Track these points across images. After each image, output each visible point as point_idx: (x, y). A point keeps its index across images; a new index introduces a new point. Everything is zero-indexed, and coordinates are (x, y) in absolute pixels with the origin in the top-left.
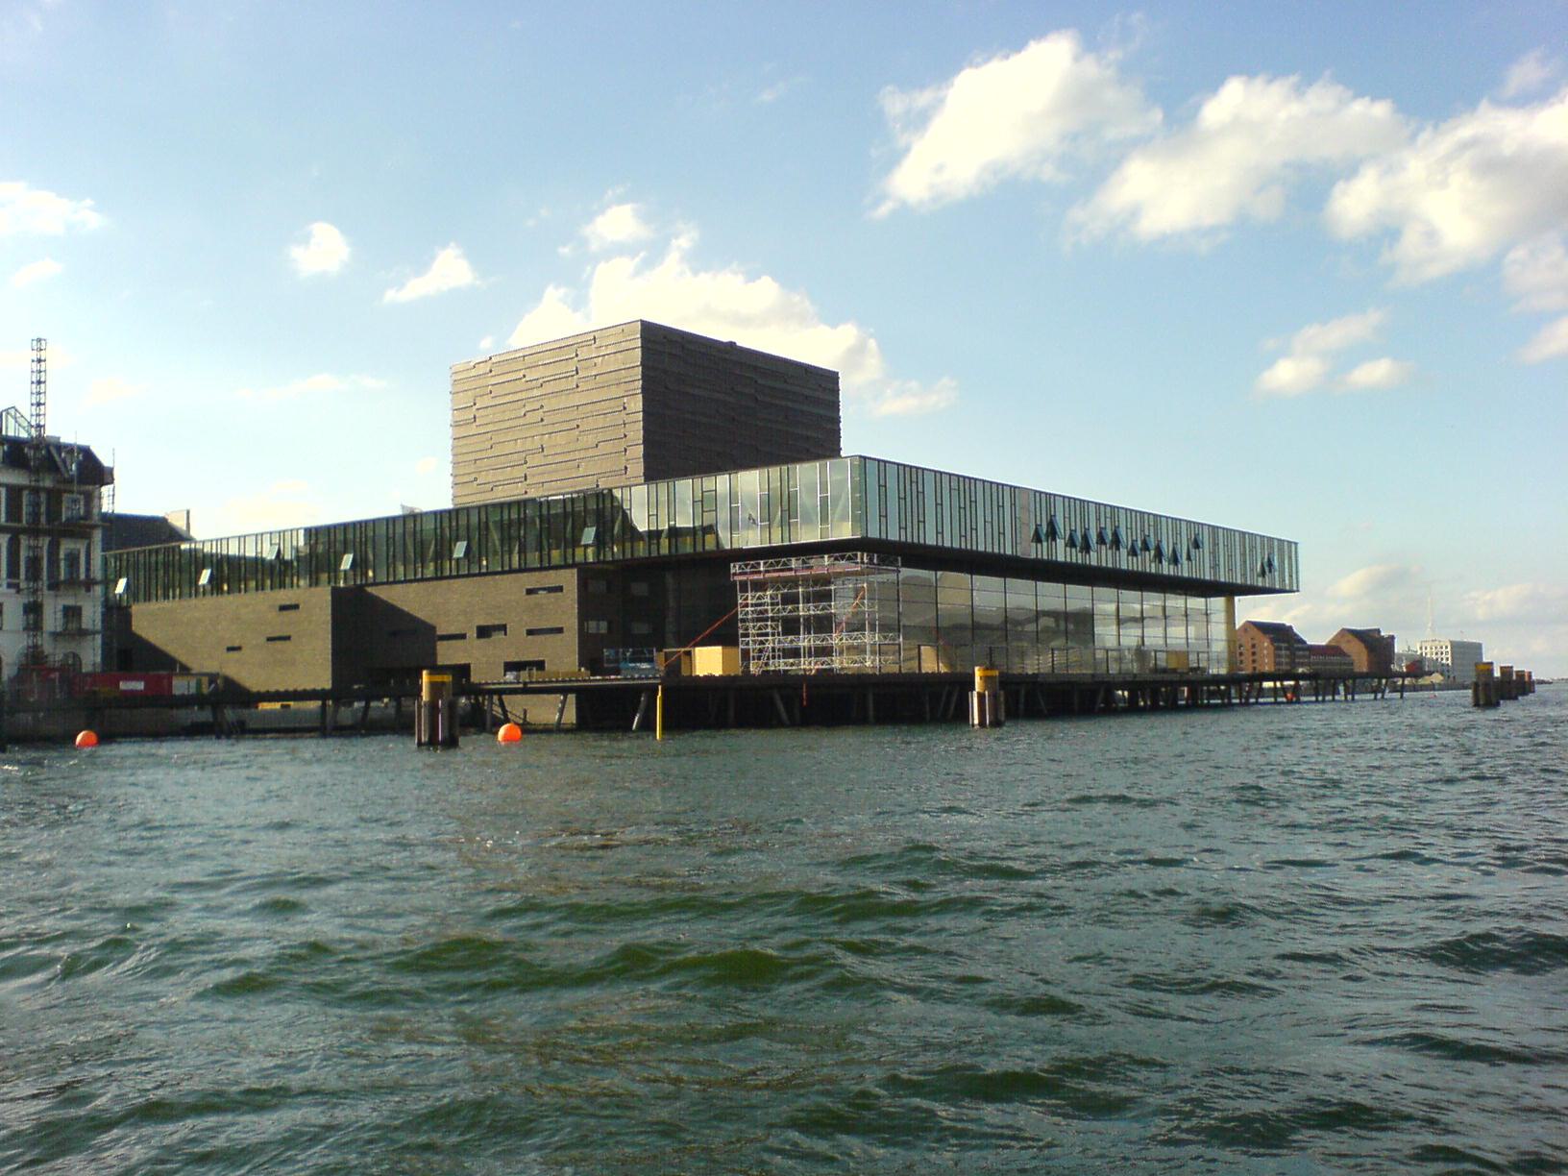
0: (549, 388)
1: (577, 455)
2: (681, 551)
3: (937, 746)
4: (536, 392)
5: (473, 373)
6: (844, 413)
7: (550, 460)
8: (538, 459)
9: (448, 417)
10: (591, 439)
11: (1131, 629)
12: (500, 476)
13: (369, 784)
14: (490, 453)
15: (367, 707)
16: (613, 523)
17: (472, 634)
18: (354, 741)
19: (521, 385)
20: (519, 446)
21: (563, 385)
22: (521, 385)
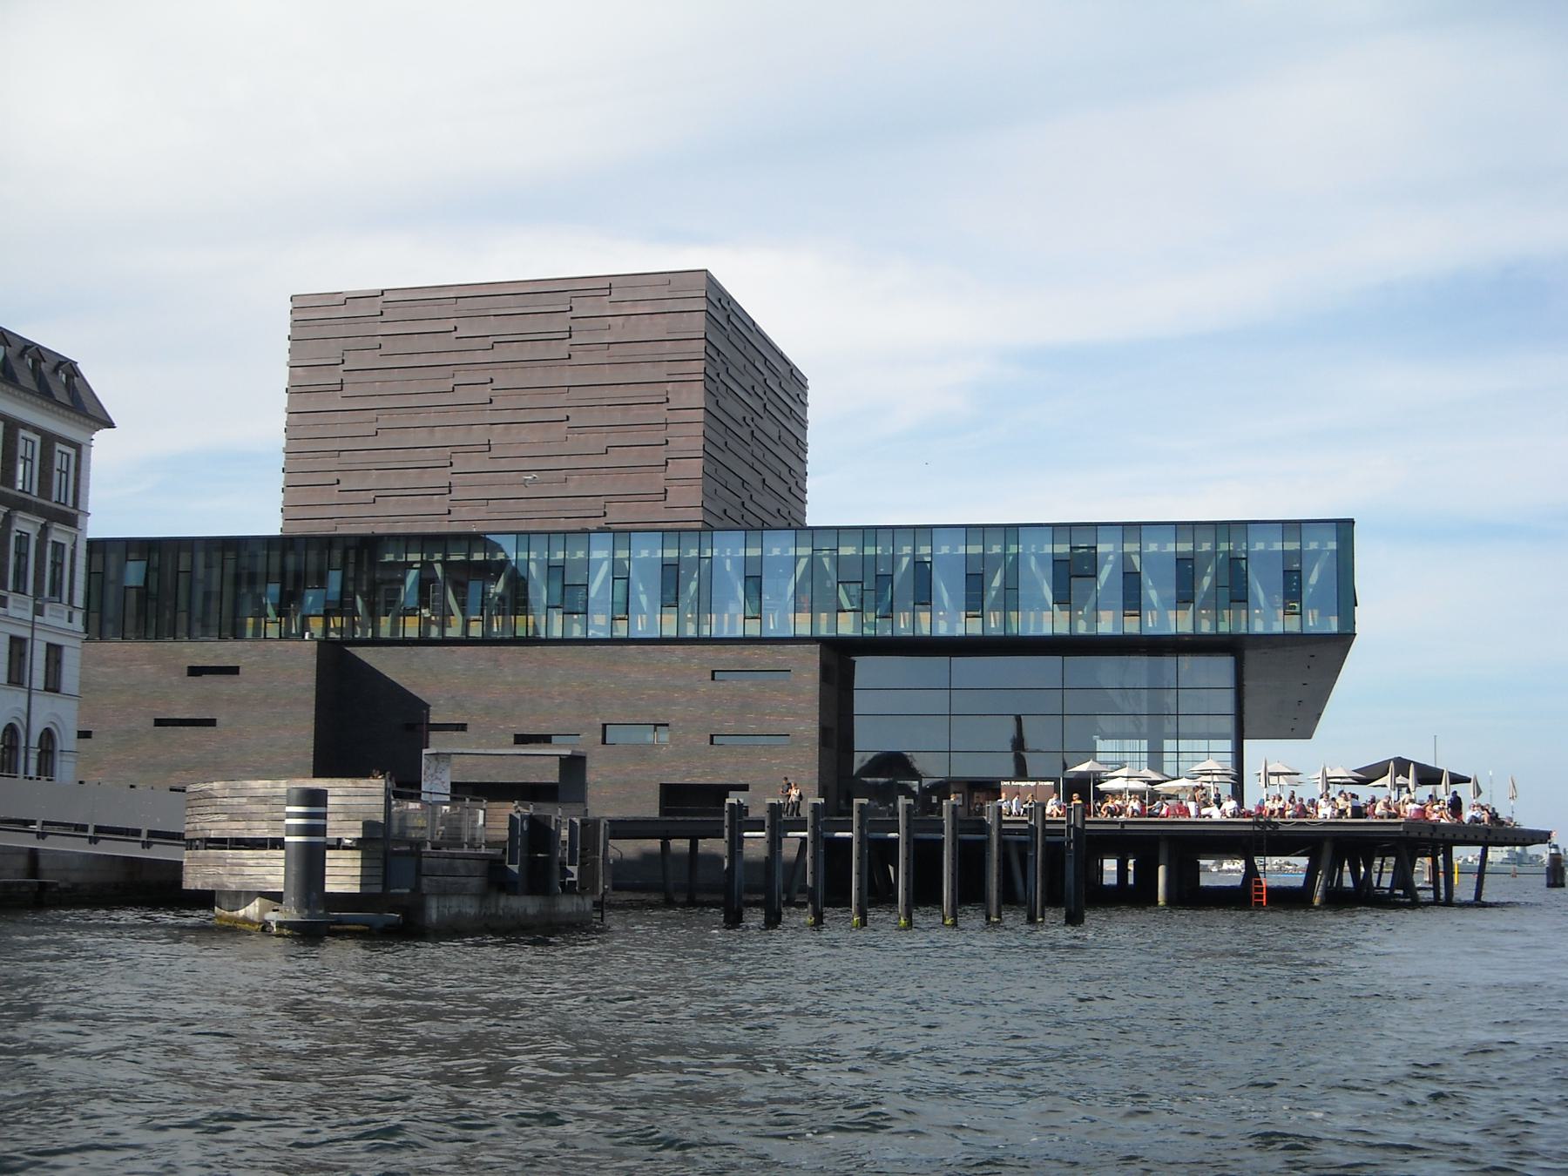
1: (563, 463)
2: (918, 633)
3: (1297, 918)
4: (480, 357)
5: (343, 311)
6: (813, 437)
7: (504, 464)
8: (478, 462)
9: (282, 377)
10: (595, 442)
11: (1168, 768)
12: (393, 480)
13: (630, 960)
14: (370, 443)
15: (694, 846)
16: (1266, 595)
18: (1116, 915)
19: (447, 342)
20: (439, 437)
21: (540, 351)
22: (447, 342)
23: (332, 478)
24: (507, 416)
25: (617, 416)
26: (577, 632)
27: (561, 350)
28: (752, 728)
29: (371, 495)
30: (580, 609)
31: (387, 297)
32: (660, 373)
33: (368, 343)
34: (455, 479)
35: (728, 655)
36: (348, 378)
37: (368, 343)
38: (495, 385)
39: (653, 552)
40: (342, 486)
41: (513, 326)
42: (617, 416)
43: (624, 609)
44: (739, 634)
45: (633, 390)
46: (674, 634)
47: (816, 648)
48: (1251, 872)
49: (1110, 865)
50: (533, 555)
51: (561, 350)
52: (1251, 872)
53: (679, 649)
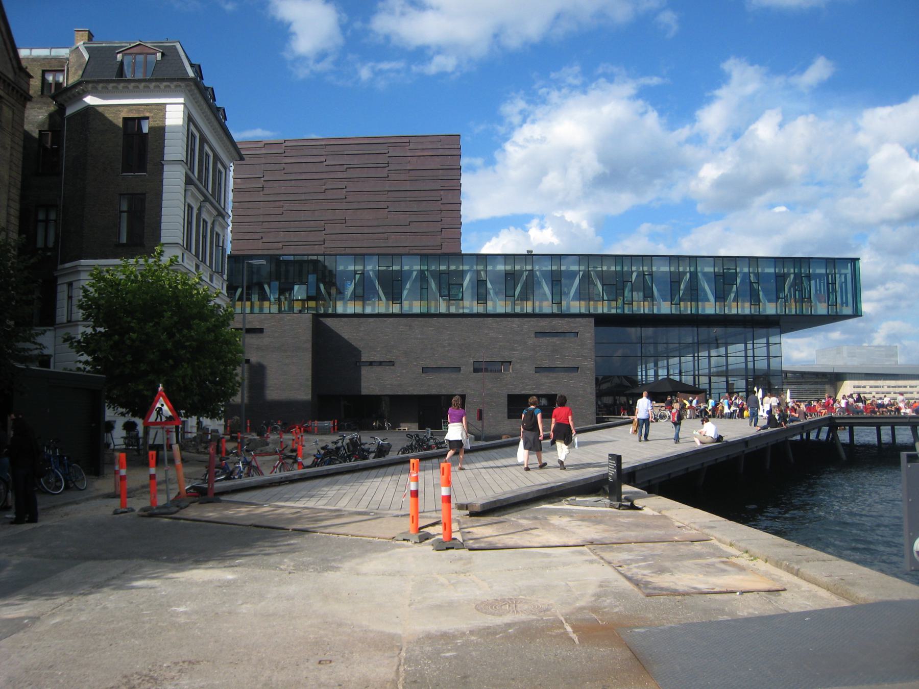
0: (349, 174)
17: (467, 369)
21: (372, 173)
23: (258, 236)
24: (355, 206)
25: (415, 207)
26: (453, 310)
27: (384, 173)
28: (558, 364)
29: (280, 245)
30: (848, 311)
31: (287, 144)
32: (437, 185)
33: (277, 167)
34: (327, 237)
35: (544, 324)
36: (266, 185)
37: (277, 167)
38: (347, 190)
39: (609, 267)
40: (264, 240)
41: (356, 160)
42: (415, 207)
43: (482, 298)
44: (475, 311)
45: (423, 194)
46: (419, 312)
47: (592, 320)
48: (615, 400)
49: (12, 323)
50: (634, 268)
51: (384, 173)
52: (615, 400)
53: (516, 320)
